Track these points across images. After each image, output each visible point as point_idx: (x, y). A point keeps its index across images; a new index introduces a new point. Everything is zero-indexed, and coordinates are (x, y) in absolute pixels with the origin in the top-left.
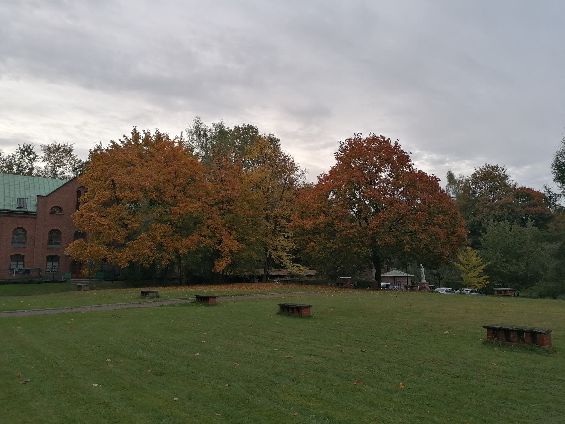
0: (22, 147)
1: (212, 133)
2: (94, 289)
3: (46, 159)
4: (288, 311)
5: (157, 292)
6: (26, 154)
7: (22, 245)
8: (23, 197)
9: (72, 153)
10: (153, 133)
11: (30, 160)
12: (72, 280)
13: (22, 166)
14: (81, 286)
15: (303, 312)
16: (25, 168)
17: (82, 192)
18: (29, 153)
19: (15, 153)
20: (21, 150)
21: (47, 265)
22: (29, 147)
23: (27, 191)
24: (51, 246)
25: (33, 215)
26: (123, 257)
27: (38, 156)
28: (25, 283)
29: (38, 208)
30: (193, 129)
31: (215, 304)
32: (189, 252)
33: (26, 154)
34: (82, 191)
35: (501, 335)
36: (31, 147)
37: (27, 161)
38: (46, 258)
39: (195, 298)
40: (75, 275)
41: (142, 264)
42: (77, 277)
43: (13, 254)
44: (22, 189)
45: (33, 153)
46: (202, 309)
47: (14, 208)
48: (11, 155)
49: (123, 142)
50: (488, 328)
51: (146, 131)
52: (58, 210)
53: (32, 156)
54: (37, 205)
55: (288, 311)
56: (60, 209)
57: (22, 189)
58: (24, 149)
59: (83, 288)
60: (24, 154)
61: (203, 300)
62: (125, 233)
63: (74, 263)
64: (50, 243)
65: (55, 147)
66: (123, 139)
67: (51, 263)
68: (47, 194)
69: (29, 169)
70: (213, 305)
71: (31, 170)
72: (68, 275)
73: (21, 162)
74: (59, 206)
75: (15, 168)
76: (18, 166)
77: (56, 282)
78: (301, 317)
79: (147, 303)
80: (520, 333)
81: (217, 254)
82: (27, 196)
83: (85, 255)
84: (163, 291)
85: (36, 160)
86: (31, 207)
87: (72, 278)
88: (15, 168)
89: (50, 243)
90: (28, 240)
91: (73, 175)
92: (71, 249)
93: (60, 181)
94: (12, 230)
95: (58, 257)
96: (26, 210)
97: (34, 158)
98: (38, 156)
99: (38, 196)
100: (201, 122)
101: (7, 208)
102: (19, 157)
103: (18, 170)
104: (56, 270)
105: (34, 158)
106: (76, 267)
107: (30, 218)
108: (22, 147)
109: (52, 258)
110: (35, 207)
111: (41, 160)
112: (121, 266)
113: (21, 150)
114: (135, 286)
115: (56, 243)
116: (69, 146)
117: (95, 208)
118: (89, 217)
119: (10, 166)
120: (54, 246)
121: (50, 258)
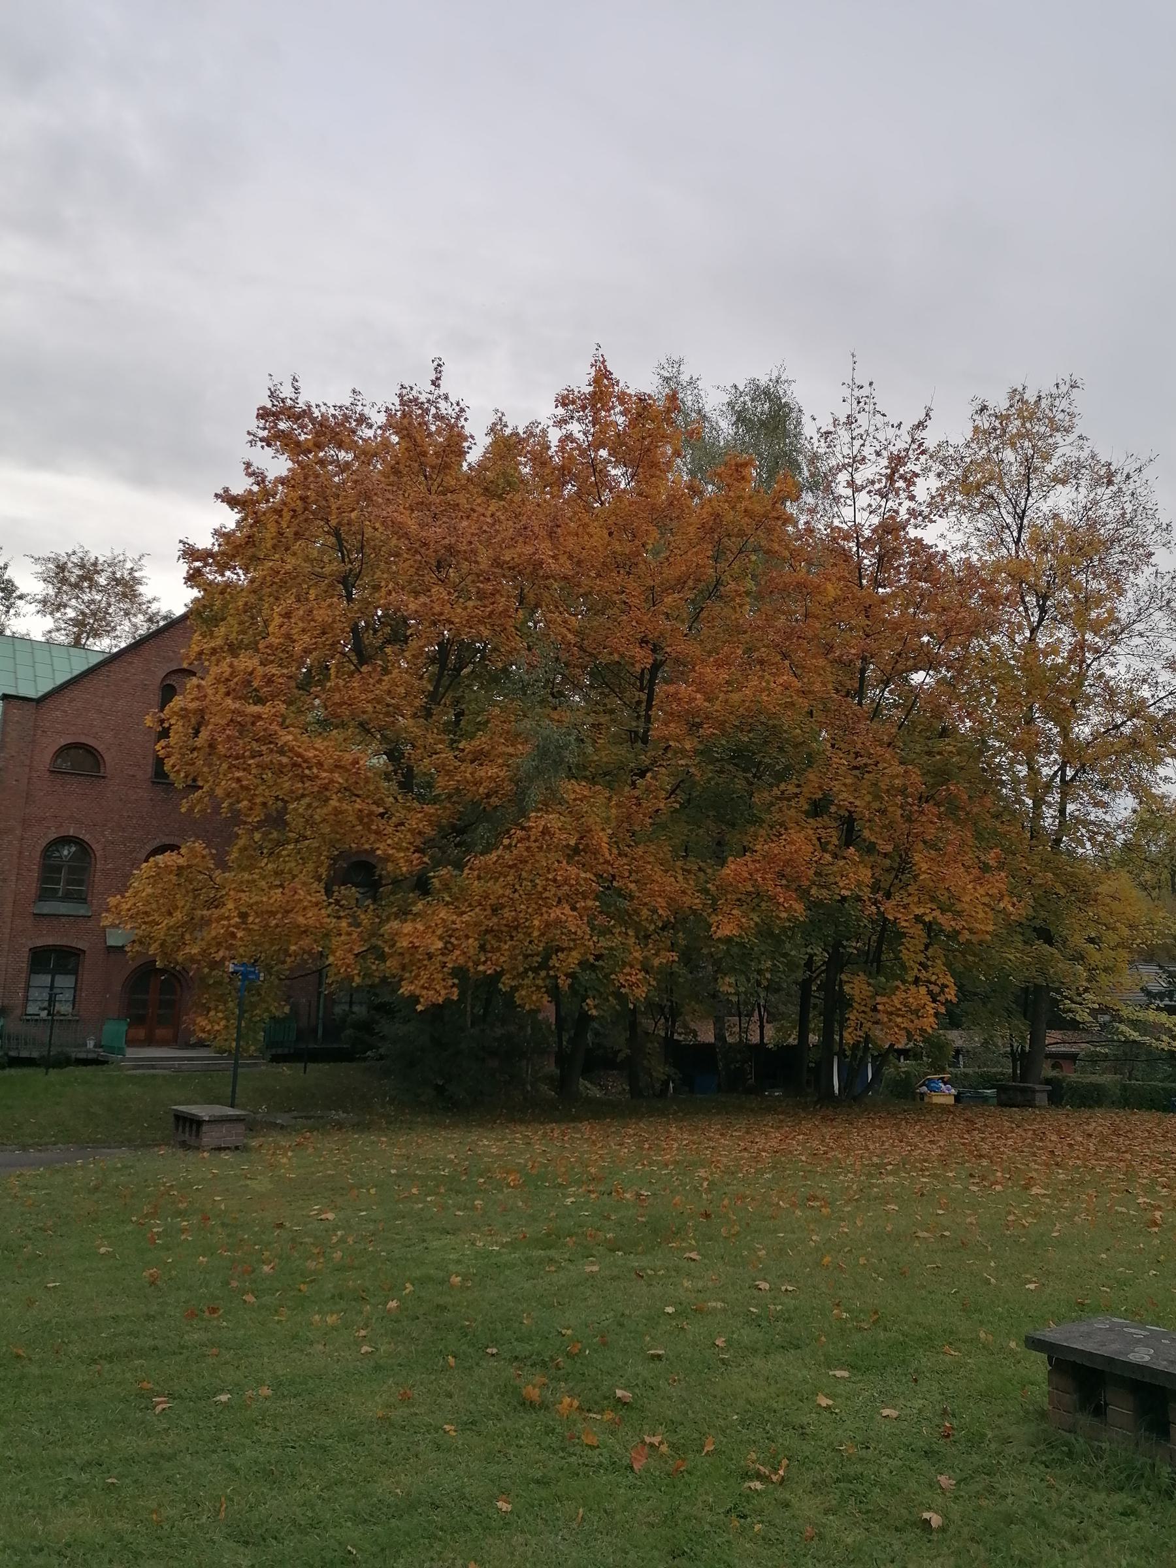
3: (49, 606)
9: (141, 589)
12: (132, 1053)
14: (193, 1124)
21: (28, 987)
24: (47, 908)
26: (429, 947)
32: (765, 932)
38: (25, 954)
40: (141, 1033)
41: (515, 989)
42: (150, 1041)
59: (210, 1136)
62: (419, 819)
63: (145, 973)
64: (45, 895)
65: (82, 566)
67: (46, 979)
68: (45, 687)
72: (116, 1029)
74: (83, 739)
77: (62, 1062)
81: (880, 951)
83: (216, 930)
87: (131, 1043)
89: (45, 895)
92: (130, 912)
95: (77, 953)
104: (64, 1008)
106: (155, 995)
109: (51, 960)
111: (33, 608)
112: (415, 999)
115: (68, 897)
116: (129, 565)
117: (270, 681)
118: (241, 725)
120: (63, 908)
121: (45, 960)
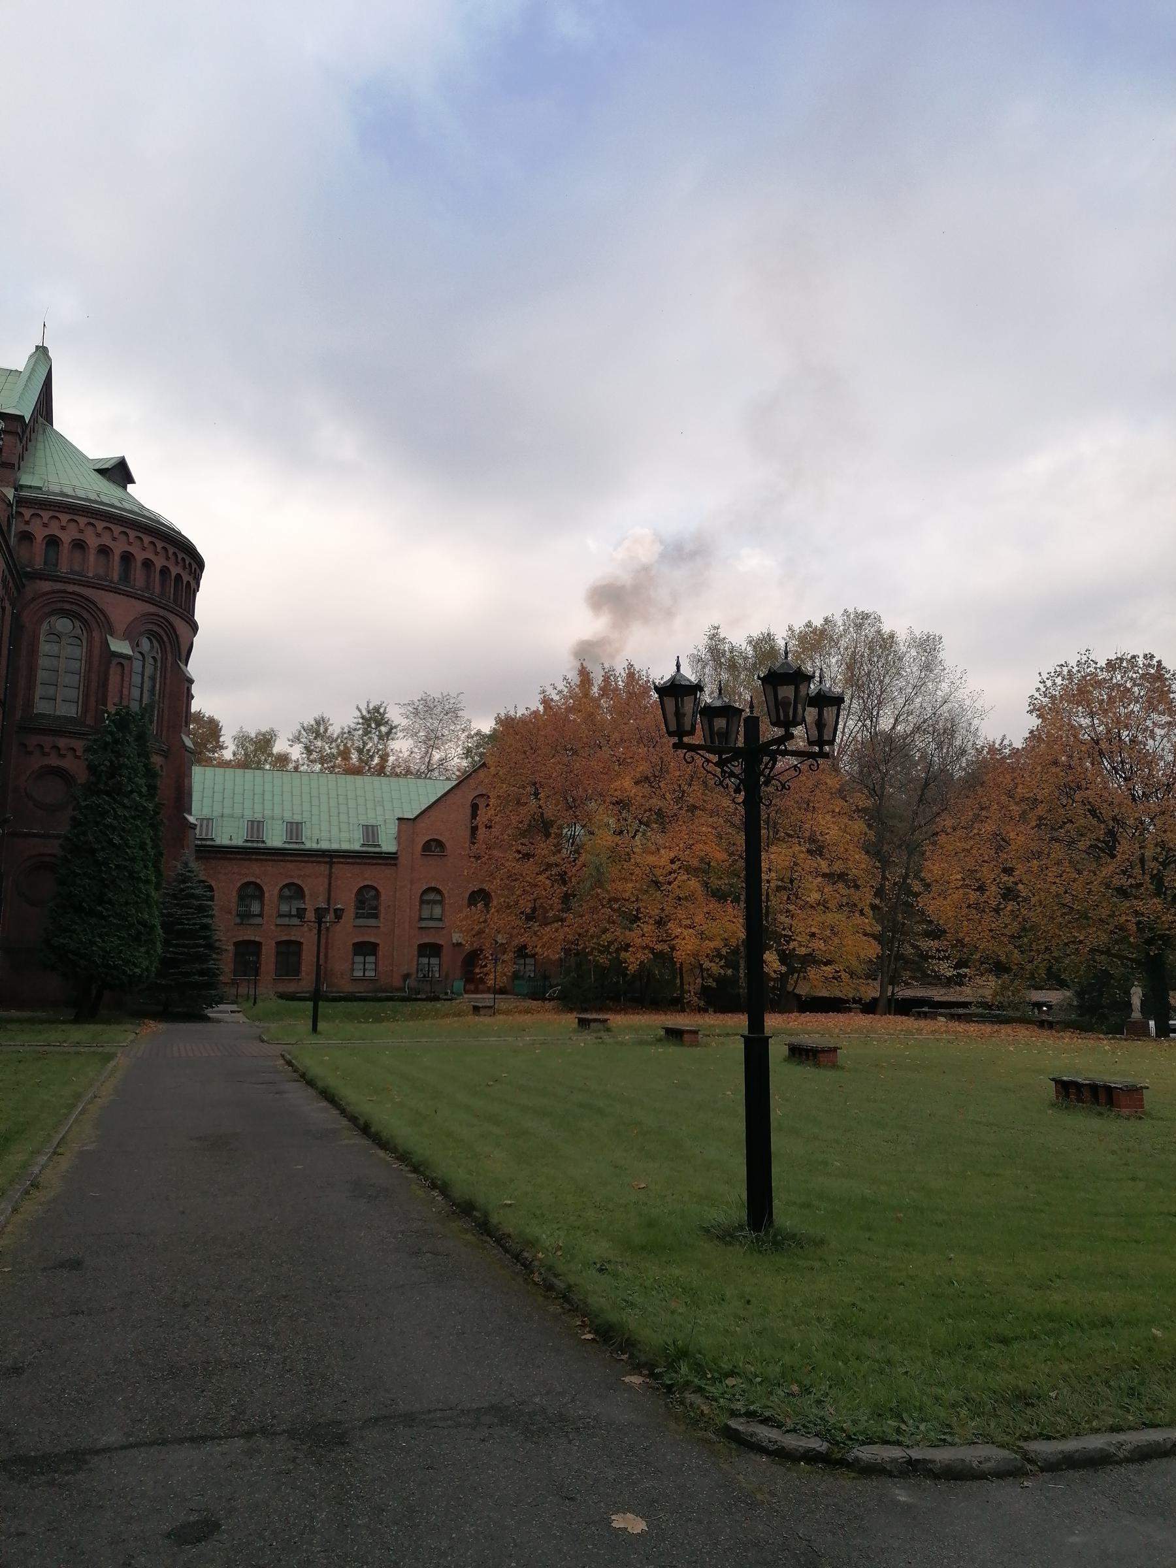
0: (365, 713)
1: (746, 658)
2: (1041, 989)
4: (800, 1054)
5: (606, 1020)
6: (373, 725)
7: (372, 922)
8: (372, 822)
9: (460, 713)
10: (620, 670)
11: (381, 737)
13: (369, 751)
15: (822, 1058)
16: (372, 757)
17: (482, 806)
18: (379, 724)
19: (353, 726)
20: (363, 717)
22: (377, 709)
23: (379, 809)
25: (389, 859)
27: (396, 727)
28: (379, 1000)
29: (399, 844)
30: (704, 653)
31: (696, 1044)
33: (373, 725)
34: (481, 803)
35: (1073, 1093)
36: (382, 710)
37: (376, 739)
39: (663, 1033)
40: (472, 987)
42: (476, 991)
43: (356, 940)
44: (370, 805)
45: (387, 723)
46: (672, 1051)
47: (356, 847)
48: (346, 730)
49: (560, 692)
50: (1057, 1082)
51: (607, 666)
52: (434, 847)
53: (384, 729)
54: (398, 838)
55: (800, 1054)
56: (440, 844)
57: (370, 805)
58: (368, 716)
60: (369, 726)
61: (675, 1035)
66: (561, 686)
69: (380, 757)
70: (691, 1045)
71: (384, 758)
73: (365, 744)
75: (354, 756)
76: (360, 751)
78: (817, 1065)
79: (586, 1039)
80: (1094, 1088)
82: (379, 821)
84: (617, 1020)
85: (392, 736)
86: (388, 844)
87: (466, 992)
88: (354, 756)
90: (383, 910)
91: (465, 763)
93: (439, 784)
94: (355, 891)
96: (377, 850)
97: (389, 733)
98: (396, 727)
99: (399, 819)
100: (722, 636)
101: (345, 846)
102: (360, 732)
103: (360, 760)
105: (389, 733)
107: (386, 865)
108: (365, 713)
110: (395, 842)
113: (363, 717)
114: (571, 1010)
119: (345, 755)
